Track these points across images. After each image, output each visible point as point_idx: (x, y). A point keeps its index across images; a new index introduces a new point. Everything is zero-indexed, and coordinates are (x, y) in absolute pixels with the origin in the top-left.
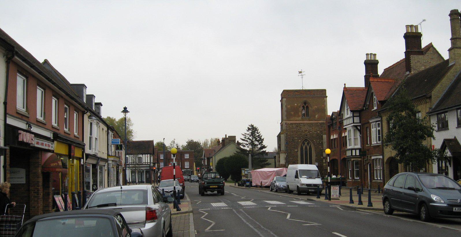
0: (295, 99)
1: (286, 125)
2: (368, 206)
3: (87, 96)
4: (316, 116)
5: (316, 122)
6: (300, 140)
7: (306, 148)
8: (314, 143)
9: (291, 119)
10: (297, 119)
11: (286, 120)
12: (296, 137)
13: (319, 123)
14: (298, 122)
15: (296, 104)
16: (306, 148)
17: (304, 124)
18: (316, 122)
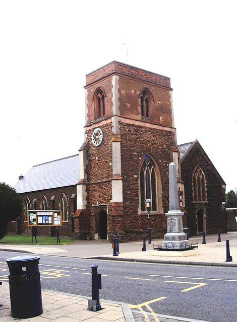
0: (132, 81)
1: (87, 135)
2: (227, 261)
3: (150, 199)
4: (161, 118)
5: (161, 128)
6: (140, 158)
7: (199, 178)
8: (159, 164)
9: (128, 116)
10: (136, 117)
11: (119, 115)
12: (135, 151)
13: (165, 131)
14: (137, 123)
15: (133, 91)
16: (199, 178)
17: (147, 130)
18: (161, 128)
